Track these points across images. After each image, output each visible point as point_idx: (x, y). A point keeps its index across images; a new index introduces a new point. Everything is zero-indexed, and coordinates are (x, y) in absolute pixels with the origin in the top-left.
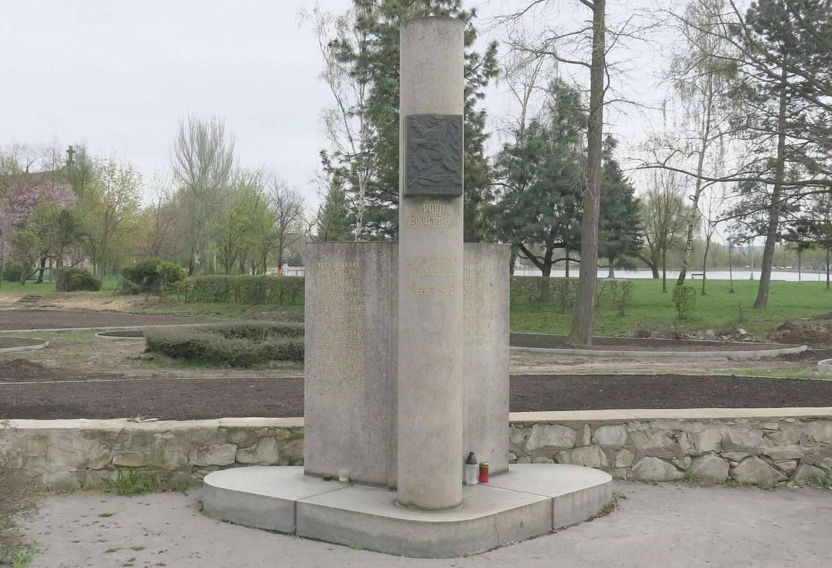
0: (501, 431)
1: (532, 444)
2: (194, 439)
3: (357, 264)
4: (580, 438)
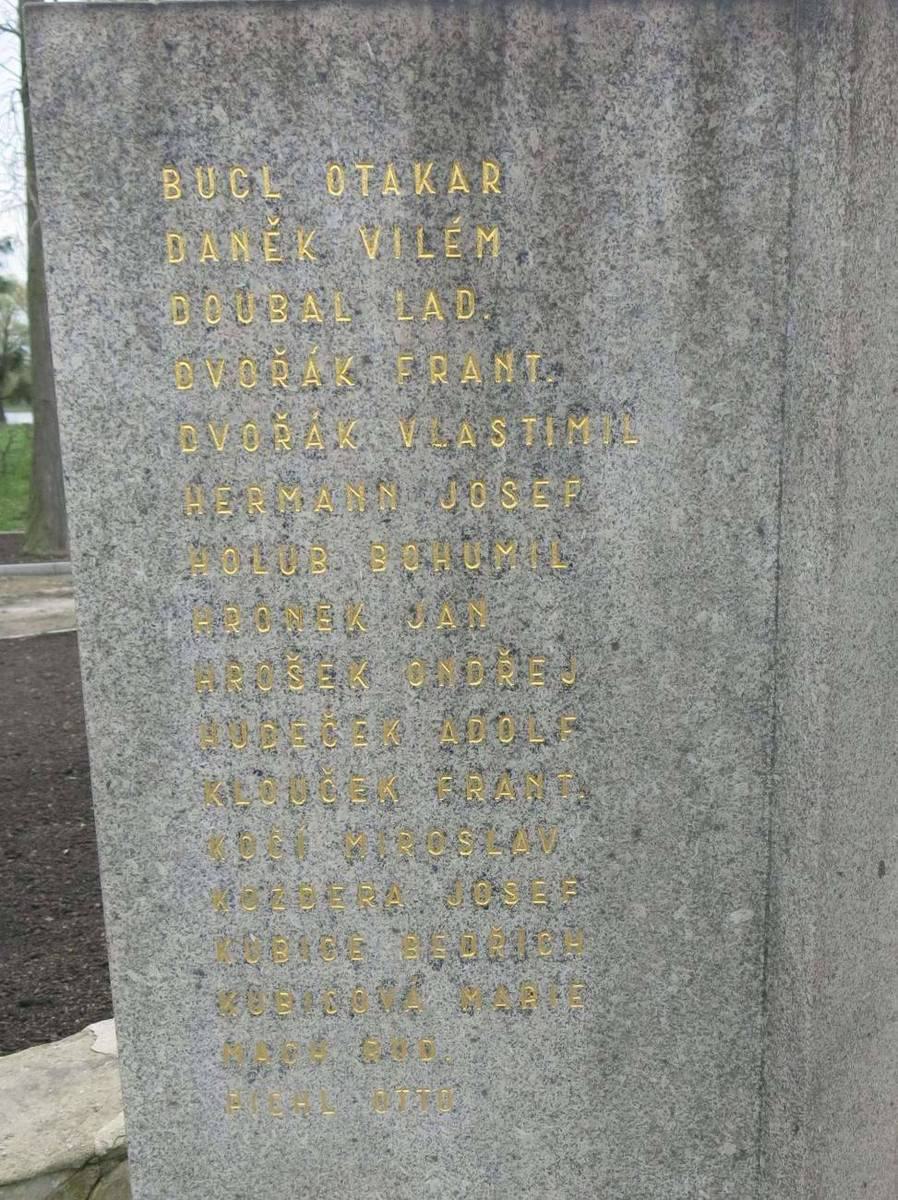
3: (516, 172)
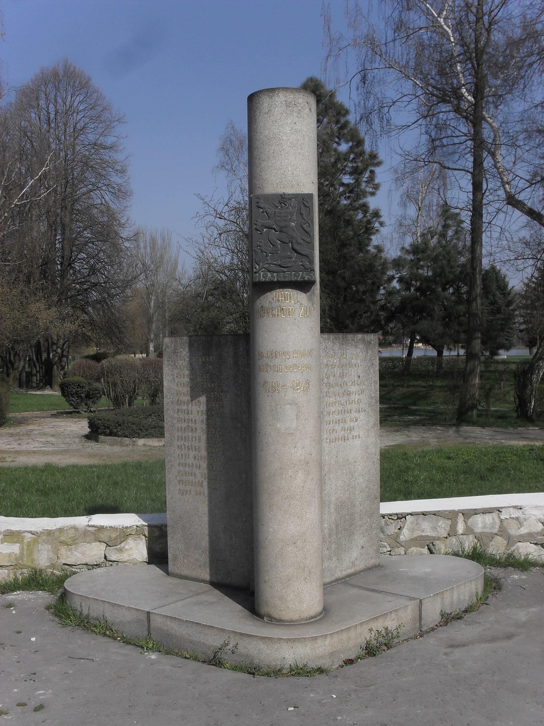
0: (371, 526)
1: (405, 535)
2: (62, 538)
4: (453, 527)
